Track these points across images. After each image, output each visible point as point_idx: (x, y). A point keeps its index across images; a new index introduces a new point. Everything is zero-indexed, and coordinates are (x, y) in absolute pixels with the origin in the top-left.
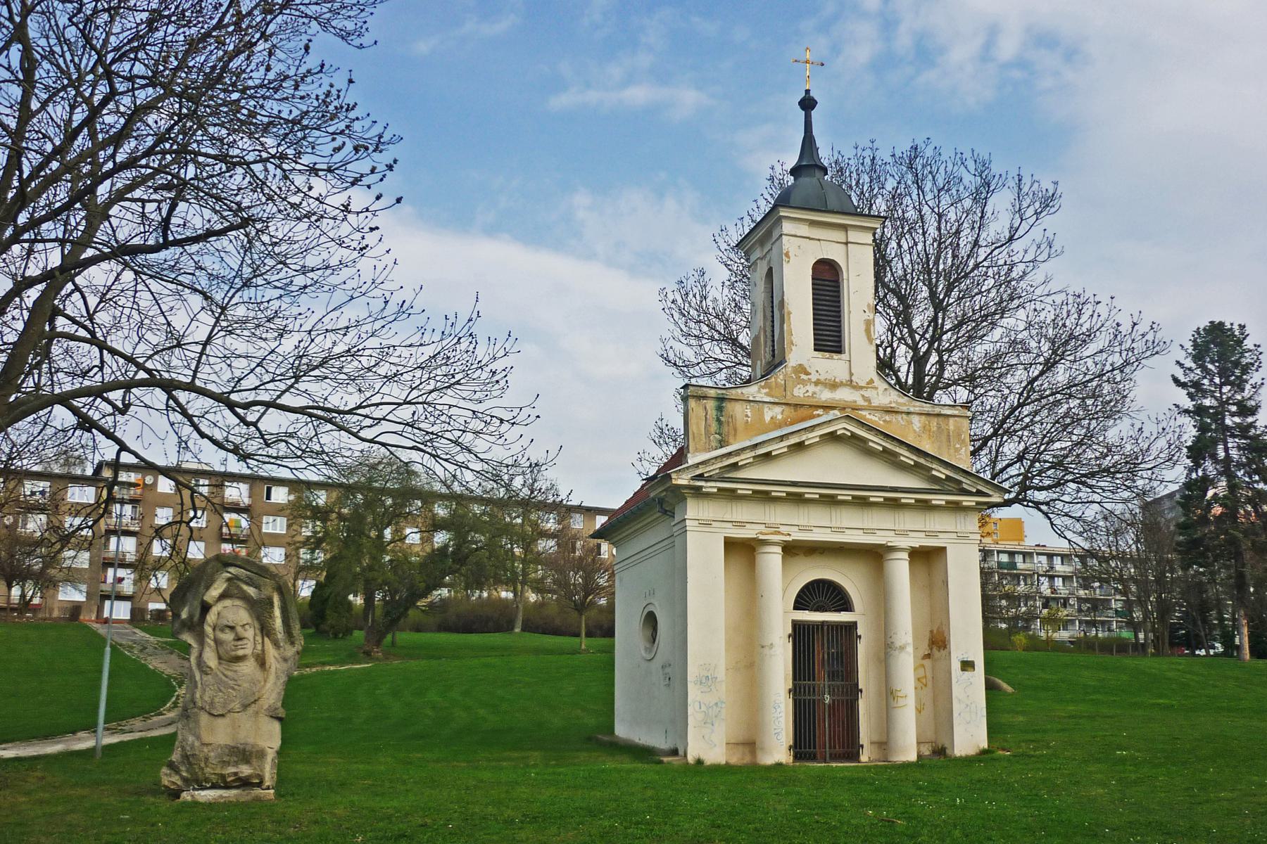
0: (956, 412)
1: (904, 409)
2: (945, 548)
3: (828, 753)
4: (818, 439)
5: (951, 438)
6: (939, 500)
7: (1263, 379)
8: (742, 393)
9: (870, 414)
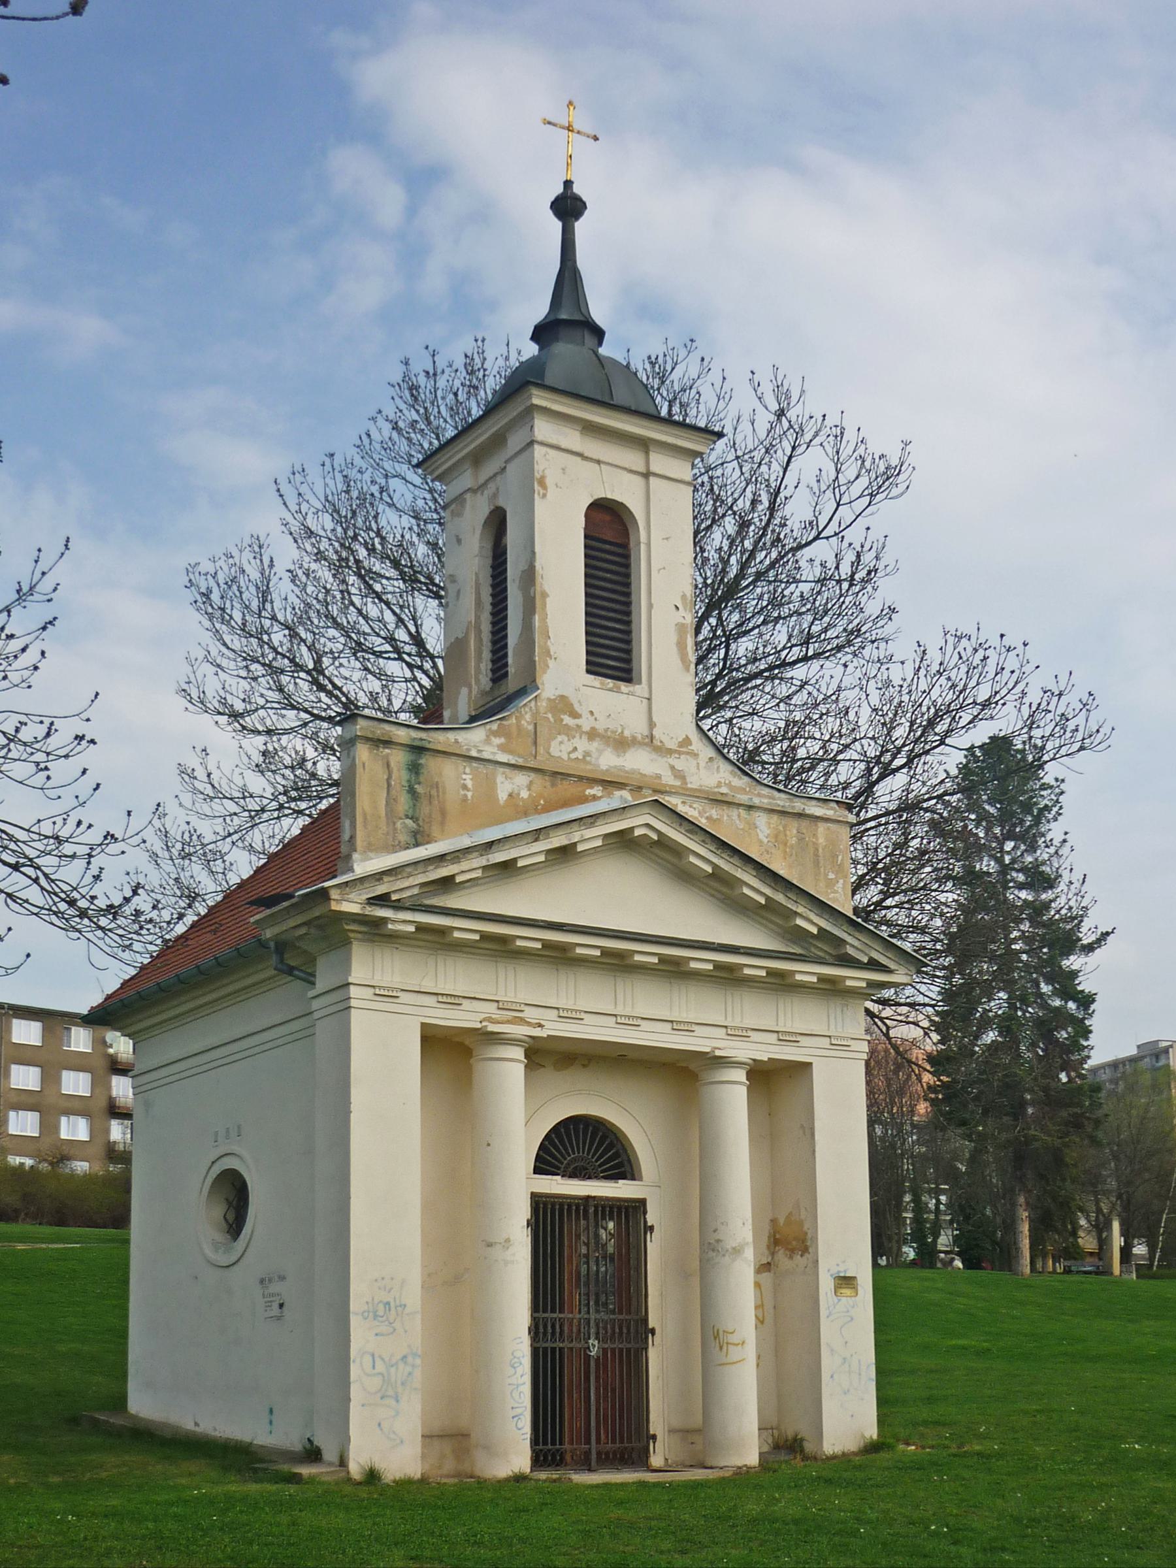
0: (830, 813)
1: (743, 798)
2: (809, 1065)
3: (594, 1452)
4: (599, 843)
5: (821, 859)
6: (807, 973)
7: (1066, 833)
8: (456, 741)
9: (683, 803)
